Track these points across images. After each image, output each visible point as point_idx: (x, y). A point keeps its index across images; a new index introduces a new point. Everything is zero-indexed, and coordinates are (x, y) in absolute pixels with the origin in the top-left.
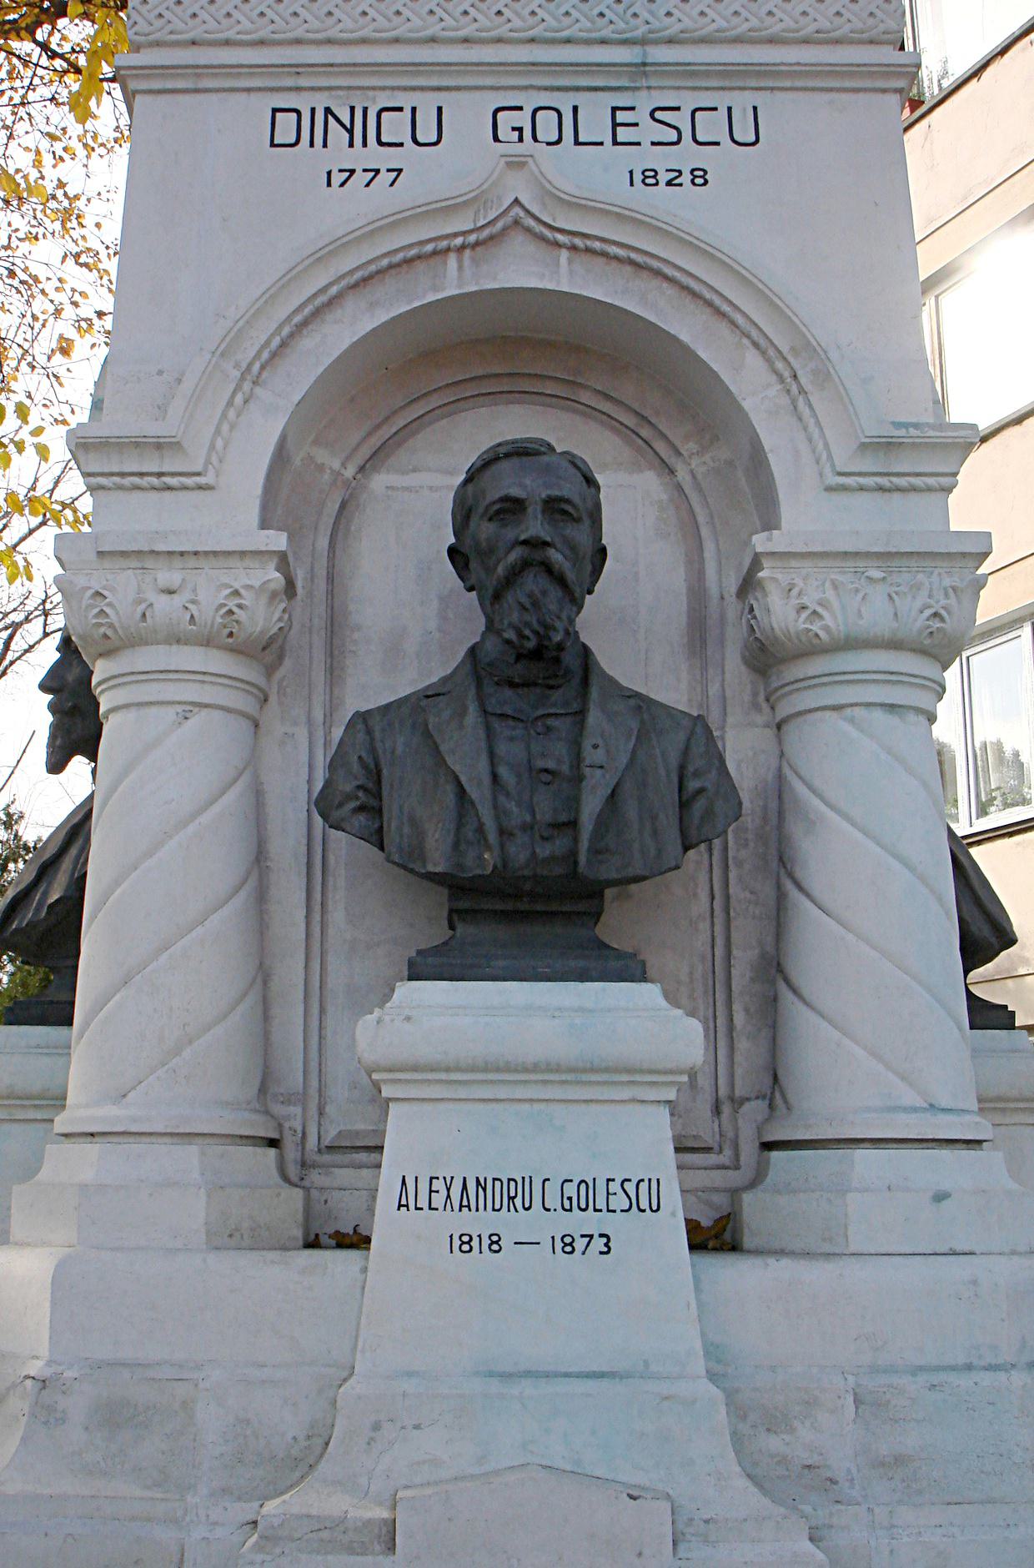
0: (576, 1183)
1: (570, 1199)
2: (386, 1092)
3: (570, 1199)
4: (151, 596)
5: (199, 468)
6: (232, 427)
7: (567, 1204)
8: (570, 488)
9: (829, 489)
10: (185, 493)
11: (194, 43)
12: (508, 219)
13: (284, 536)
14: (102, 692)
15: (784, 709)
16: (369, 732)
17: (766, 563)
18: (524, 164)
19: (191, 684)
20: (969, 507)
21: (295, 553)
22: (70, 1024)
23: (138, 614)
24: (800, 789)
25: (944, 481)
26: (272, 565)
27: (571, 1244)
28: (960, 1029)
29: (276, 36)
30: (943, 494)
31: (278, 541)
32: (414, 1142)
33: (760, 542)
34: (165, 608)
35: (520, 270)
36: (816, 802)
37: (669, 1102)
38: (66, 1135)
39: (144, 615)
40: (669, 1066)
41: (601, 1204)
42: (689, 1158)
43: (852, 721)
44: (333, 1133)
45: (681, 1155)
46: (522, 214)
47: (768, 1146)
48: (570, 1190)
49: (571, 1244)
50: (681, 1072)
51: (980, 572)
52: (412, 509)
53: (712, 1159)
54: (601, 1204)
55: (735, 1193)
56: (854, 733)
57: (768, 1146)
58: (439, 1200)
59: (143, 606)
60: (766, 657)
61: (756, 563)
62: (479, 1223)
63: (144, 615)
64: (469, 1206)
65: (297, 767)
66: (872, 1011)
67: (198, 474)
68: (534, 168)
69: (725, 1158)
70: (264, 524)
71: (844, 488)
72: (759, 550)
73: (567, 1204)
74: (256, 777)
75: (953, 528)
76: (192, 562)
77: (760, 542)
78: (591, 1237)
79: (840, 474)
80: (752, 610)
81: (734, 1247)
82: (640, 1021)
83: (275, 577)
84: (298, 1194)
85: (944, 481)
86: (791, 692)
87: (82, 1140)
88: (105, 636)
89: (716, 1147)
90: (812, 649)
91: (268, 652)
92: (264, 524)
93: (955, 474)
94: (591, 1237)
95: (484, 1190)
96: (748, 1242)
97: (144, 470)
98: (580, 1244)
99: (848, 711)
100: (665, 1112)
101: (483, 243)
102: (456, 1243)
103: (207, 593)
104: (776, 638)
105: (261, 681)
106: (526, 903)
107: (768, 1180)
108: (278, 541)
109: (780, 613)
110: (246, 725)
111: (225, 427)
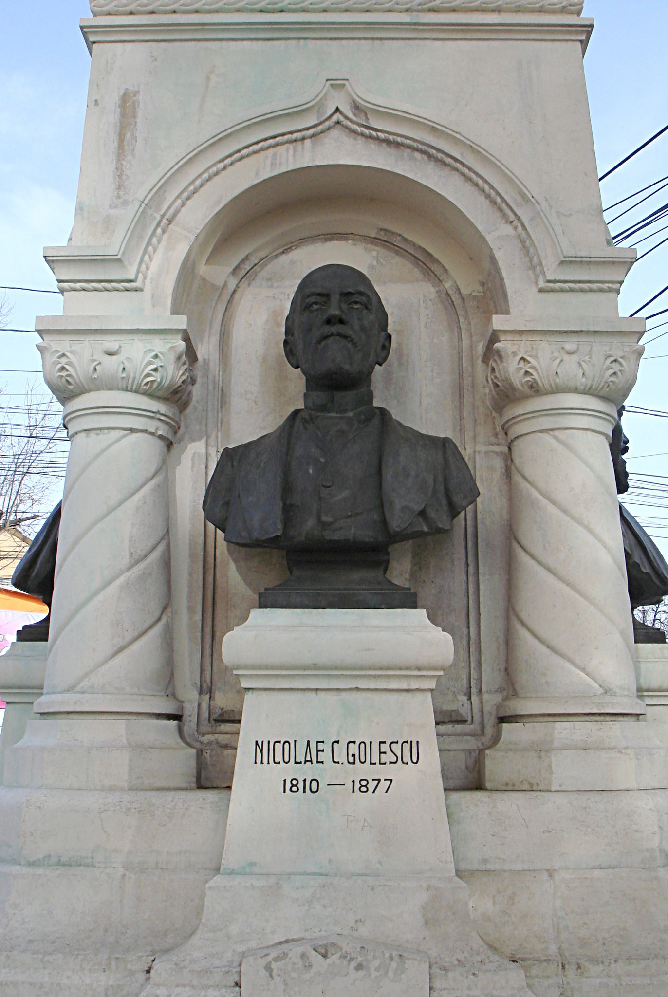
0: (357, 743)
1: (353, 755)
2: (245, 684)
3: (353, 755)
5: (132, 277)
6: (164, 232)
9: (541, 290)
11: (347, 11)
13: (185, 318)
17: (502, 338)
18: (344, 85)
22: (47, 640)
23: (92, 368)
24: (524, 485)
26: (179, 337)
27: (366, 786)
28: (625, 639)
30: (612, 295)
31: (181, 322)
32: (260, 719)
33: (498, 322)
34: (110, 365)
35: (340, 152)
36: (535, 494)
37: (432, 690)
38: (42, 714)
41: (375, 759)
42: (449, 728)
43: (556, 438)
44: (218, 711)
45: (439, 727)
46: (341, 118)
47: (502, 720)
49: (366, 786)
51: (641, 343)
52: (261, 314)
54: (375, 759)
55: (481, 752)
56: (560, 448)
58: (325, 756)
60: (505, 396)
61: (494, 337)
63: (95, 369)
64: (311, 761)
65: (194, 470)
66: (583, 627)
67: (131, 281)
68: (349, 89)
70: (175, 311)
71: (552, 290)
73: (351, 759)
74: (166, 479)
77: (498, 322)
78: (379, 780)
79: (549, 281)
80: (493, 370)
82: (408, 634)
83: (182, 345)
86: (518, 422)
89: (470, 720)
90: (535, 390)
91: (176, 397)
92: (175, 311)
93: (621, 283)
94: (379, 780)
95: (262, 751)
96: (488, 785)
98: (372, 785)
99: (556, 433)
101: (316, 135)
104: (511, 385)
107: (502, 740)
109: (512, 370)
110: (161, 443)
111: (159, 231)
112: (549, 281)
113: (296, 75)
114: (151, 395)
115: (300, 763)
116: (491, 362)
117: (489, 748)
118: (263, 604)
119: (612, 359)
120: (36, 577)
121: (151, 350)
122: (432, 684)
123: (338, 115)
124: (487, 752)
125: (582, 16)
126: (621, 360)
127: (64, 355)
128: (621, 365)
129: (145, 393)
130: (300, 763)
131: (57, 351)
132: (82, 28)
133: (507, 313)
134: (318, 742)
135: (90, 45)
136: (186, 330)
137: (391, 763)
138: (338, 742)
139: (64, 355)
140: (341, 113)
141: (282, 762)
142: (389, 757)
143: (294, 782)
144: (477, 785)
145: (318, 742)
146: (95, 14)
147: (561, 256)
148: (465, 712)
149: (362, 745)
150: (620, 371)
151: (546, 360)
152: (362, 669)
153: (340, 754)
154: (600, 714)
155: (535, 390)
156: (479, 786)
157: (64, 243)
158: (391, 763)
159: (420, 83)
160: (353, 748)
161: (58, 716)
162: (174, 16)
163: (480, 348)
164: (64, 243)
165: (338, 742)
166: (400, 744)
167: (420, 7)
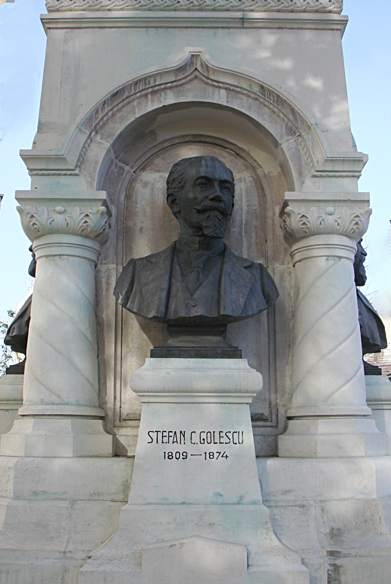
3: (204, 439)
4: (324, 216)
5: (73, 168)
7: (202, 442)
8: (225, 176)
10: (322, 178)
11: (227, 10)
12: (193, 76)
14: (37, 250)
15: (297, 257)
16: (134, 268)
17: (290, 204)
19: (324, 249)
20: (364, 185)
21: (110, 200)
22: (23, 374)
25: (356, 174)
29: (271, 8)
31: (103, 195)
33: (288, 195)
34: (59, 220)
38: (23, 416)
39: (321, 223)
40: (143, 390)
46: (198, 74)
47: (290, 418)
48: (204, 436)
50: (253, 392)
52: (152, 185)
53: (268, 424)
57: (290, 418)
59: (51, 219)
61: (286, 204)
62: (174, 448)
63: (321, 223)
69: (274, 423)
72: (286, 198)
73: (202, 442)
75: (360, 191)
76: (337, 204)
79: (317, 171)
80: (285, 221)
81: (278, 456)
82: (239, 372)
84: (111, 436)
85: (356, 174)
87: (361, 417)
88: (306, 232)
92: (101, 188)
93: (360, 172)
96: (279, 455)
97: (49, 168)
98: (216, 455)
100: (248, 406)
102: (208, 455)
103: (76, 215)
105: (98, 249)
106: (185, 332)
108: (103, 195)
109: (294, 222)
112: (317, 171)
113: (176, 50)
114: (87, 237)
115: (217, 443)
116: (284, 217)
117: (281, 434)
118: (152, 356)
119: (301, 215)
120: (18, 340)
121: (353, 214)
122: (250, 401)
123: (196, 72)
124: (280, 436)
125: (342, 14)
126: (306, 215)
127: (357, 216)
128: (307, 218)
129: (81, 235)
130: (217, 443)
131: (299, 214)
132: (41, 19)
133: (369, 193)
134: (220, 432)
135: (47, 29)
136: (105, 200)
137: (226, 443)
138: (195, 432)
139: (357, 216)
140: (198, 71)
141: (238, 443)
142: (225, 440)
143: (170, 454)
144: (275, 454)
145: (220, 432)
146: (49, 11)
147: (325, 156)
148: (266, 413)
149: (209, 434)
150: (36, 220)
151: (313, 215)
152: (186, 392)
153: (196, 438)
154: (62, 415)
155: (307, 234)
156: (275, 455)
157: (30, 148)
158: (226, 443)
159: (256, 55)
160: (204, 436)
161: (324, 418)
162: (177, 13)
163: (277, 210)
164: (30, 148)
165: (195, 432)
166: (232, 433)
167: (168, 8)
